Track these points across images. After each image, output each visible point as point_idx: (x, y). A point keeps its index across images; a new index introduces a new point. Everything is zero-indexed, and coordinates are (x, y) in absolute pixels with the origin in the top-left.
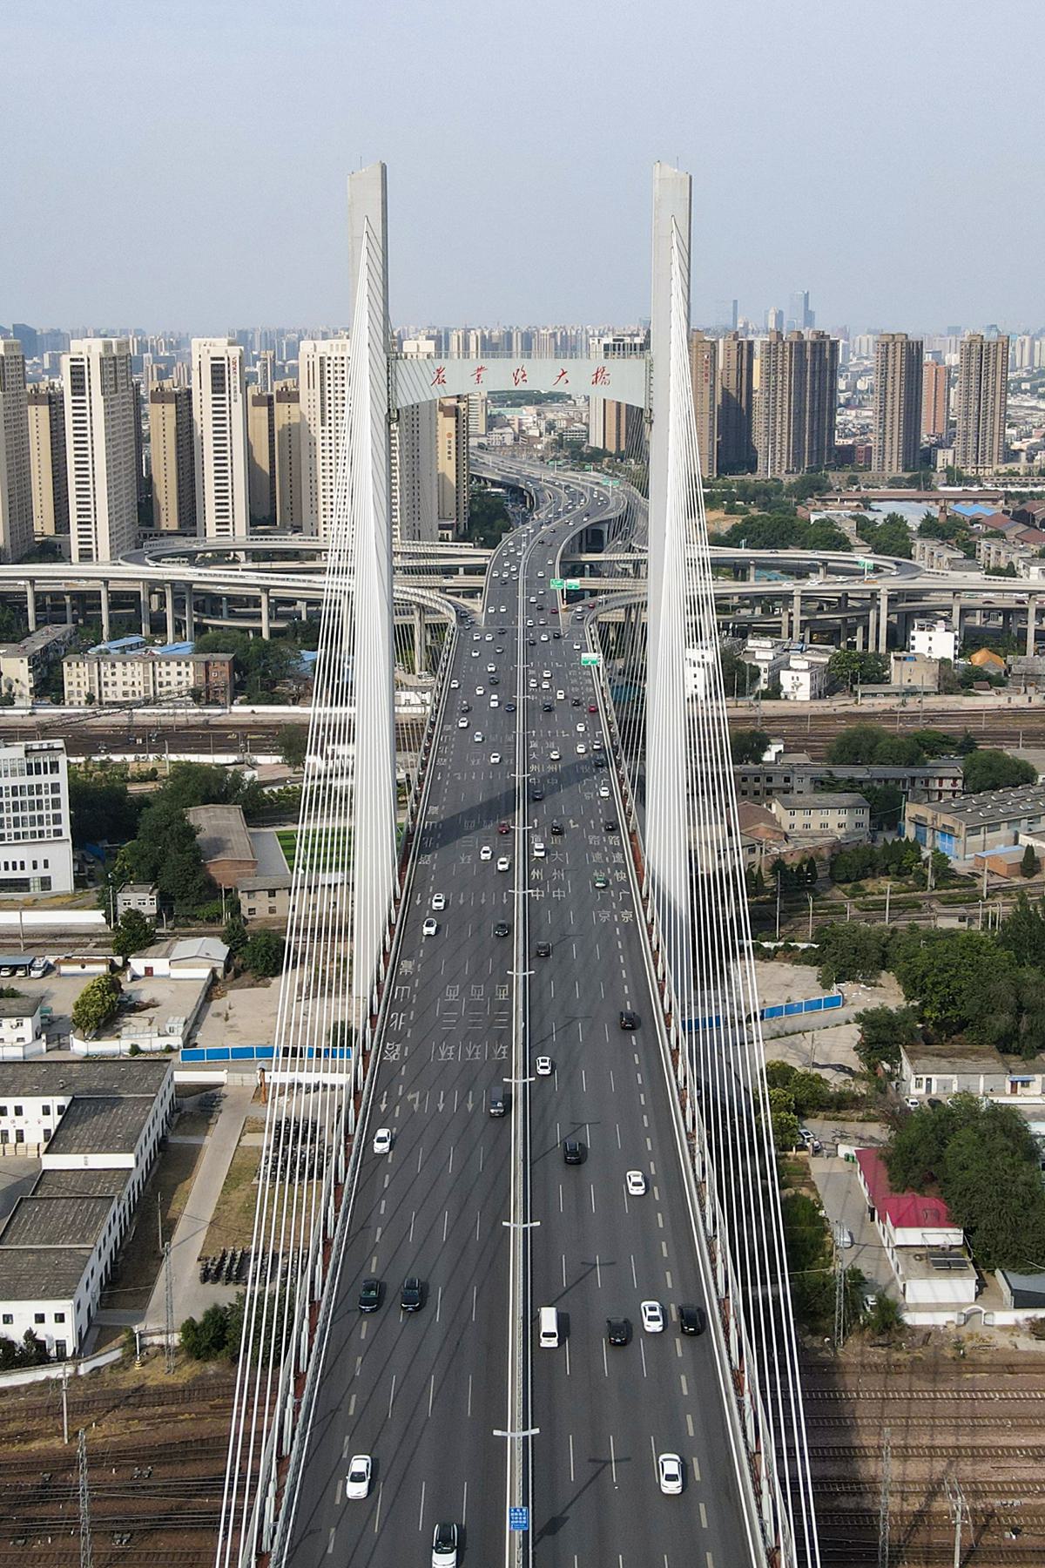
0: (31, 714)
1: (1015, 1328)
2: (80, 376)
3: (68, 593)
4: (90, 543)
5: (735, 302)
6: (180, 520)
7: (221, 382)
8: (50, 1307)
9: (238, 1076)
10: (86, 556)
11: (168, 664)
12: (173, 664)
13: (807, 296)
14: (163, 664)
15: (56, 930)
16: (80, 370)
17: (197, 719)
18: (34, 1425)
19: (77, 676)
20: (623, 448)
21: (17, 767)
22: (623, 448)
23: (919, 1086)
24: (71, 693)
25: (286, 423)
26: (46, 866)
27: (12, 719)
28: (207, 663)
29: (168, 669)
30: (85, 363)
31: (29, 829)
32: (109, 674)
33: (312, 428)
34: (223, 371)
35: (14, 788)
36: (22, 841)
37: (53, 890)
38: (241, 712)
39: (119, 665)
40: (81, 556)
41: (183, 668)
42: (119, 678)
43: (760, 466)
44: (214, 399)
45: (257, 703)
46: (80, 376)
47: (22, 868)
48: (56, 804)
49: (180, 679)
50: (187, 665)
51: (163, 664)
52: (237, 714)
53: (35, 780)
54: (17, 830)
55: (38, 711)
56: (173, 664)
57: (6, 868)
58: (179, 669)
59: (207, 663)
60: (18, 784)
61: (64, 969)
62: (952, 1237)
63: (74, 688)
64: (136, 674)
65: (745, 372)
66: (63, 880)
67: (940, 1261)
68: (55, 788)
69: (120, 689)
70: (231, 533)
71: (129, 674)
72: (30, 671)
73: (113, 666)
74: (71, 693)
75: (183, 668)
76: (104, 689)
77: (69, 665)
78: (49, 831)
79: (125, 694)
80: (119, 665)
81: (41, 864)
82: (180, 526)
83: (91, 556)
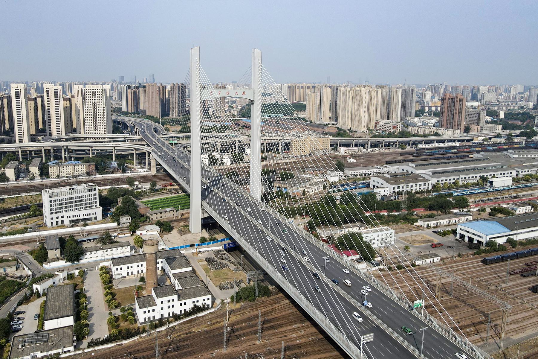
0: (42, 181)
1: (376, 270)
2: (18, 94)
3: (28, 151)
4: (22, 138)
5: (135, 76)
6: (36, 132)
7: (57, 95)
8: (206, 297)
9: (187, 251)
10: (21, 141)
11: (78, 166)
12: (80, 166)
13: (153, 75)
14: (77, 166)
15: (106, 229)
16: (18, 92)
17: (89, 179)
18: (218, 320)
19: (53, 171)
20: (133, 111)
21: (80, 191)
22: (133, 111)
23: (323, 234)
24: (51, 175)
25: (66, 106)
26: (96, 214)
27: (37, 183)
28: (89, 165)
29: (78, 167)
30: (19, 90)
31: (59, 211)
32: (62, 169)
33: (79, 107)
34: (58, 93)
35: (66, 199)
36: (91, 208)
37: (97, 220)
38: (99, 177)
39: (65, 167)
40: (19, 141)
41: (82, 167)
42: (65, 170)
43: (171, 115)
44: (16, 100)
45: (103, 174)
46: (18, 94)
47: (90, 215)
48: (95, 199)
49: (82, 169)
50: (84, 166)
51: (77, 166)
52: (99, 177)
53: (90, 193)
54: (56, 211)
55: (43, 180)
56: (80, 166)
57: (84, 216)
58: (81, 167)
59: (89, 165)
60: (86, 194)
61: (120, 236)
62: (358, 257)
63: (52, 174)
64: (70, 169)
65: (164, 93)
66: (100, 217)
67: (359, 261)
68: (95, 195)
69: (65, 173)
70: (61, 134)
71: (68, 169)
72: (39, 170)
73: (63, 167)
74: (51, 175)
75: (82, 167)
76: (61, 173)
77: (51, 168)
78: (84, 207)
79: (67, 174)
80: (65, 167)
81: (94, 214)
82: (36, 133)
83: (22, 141)
